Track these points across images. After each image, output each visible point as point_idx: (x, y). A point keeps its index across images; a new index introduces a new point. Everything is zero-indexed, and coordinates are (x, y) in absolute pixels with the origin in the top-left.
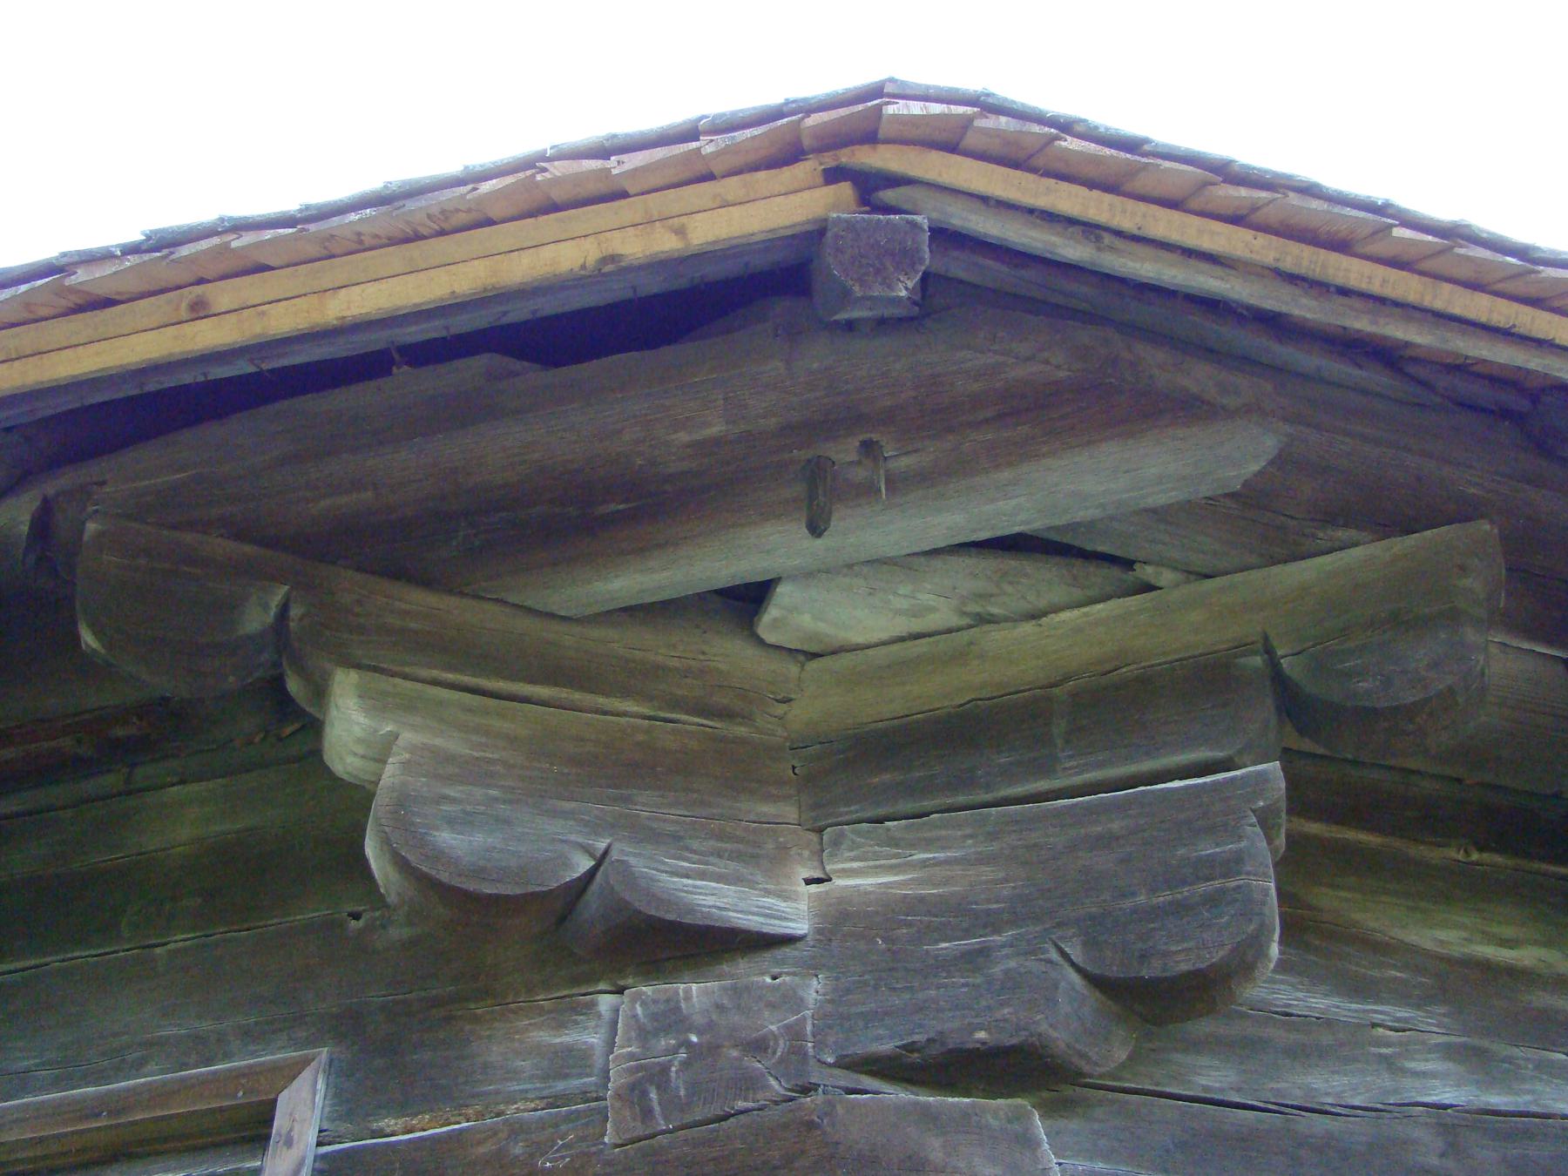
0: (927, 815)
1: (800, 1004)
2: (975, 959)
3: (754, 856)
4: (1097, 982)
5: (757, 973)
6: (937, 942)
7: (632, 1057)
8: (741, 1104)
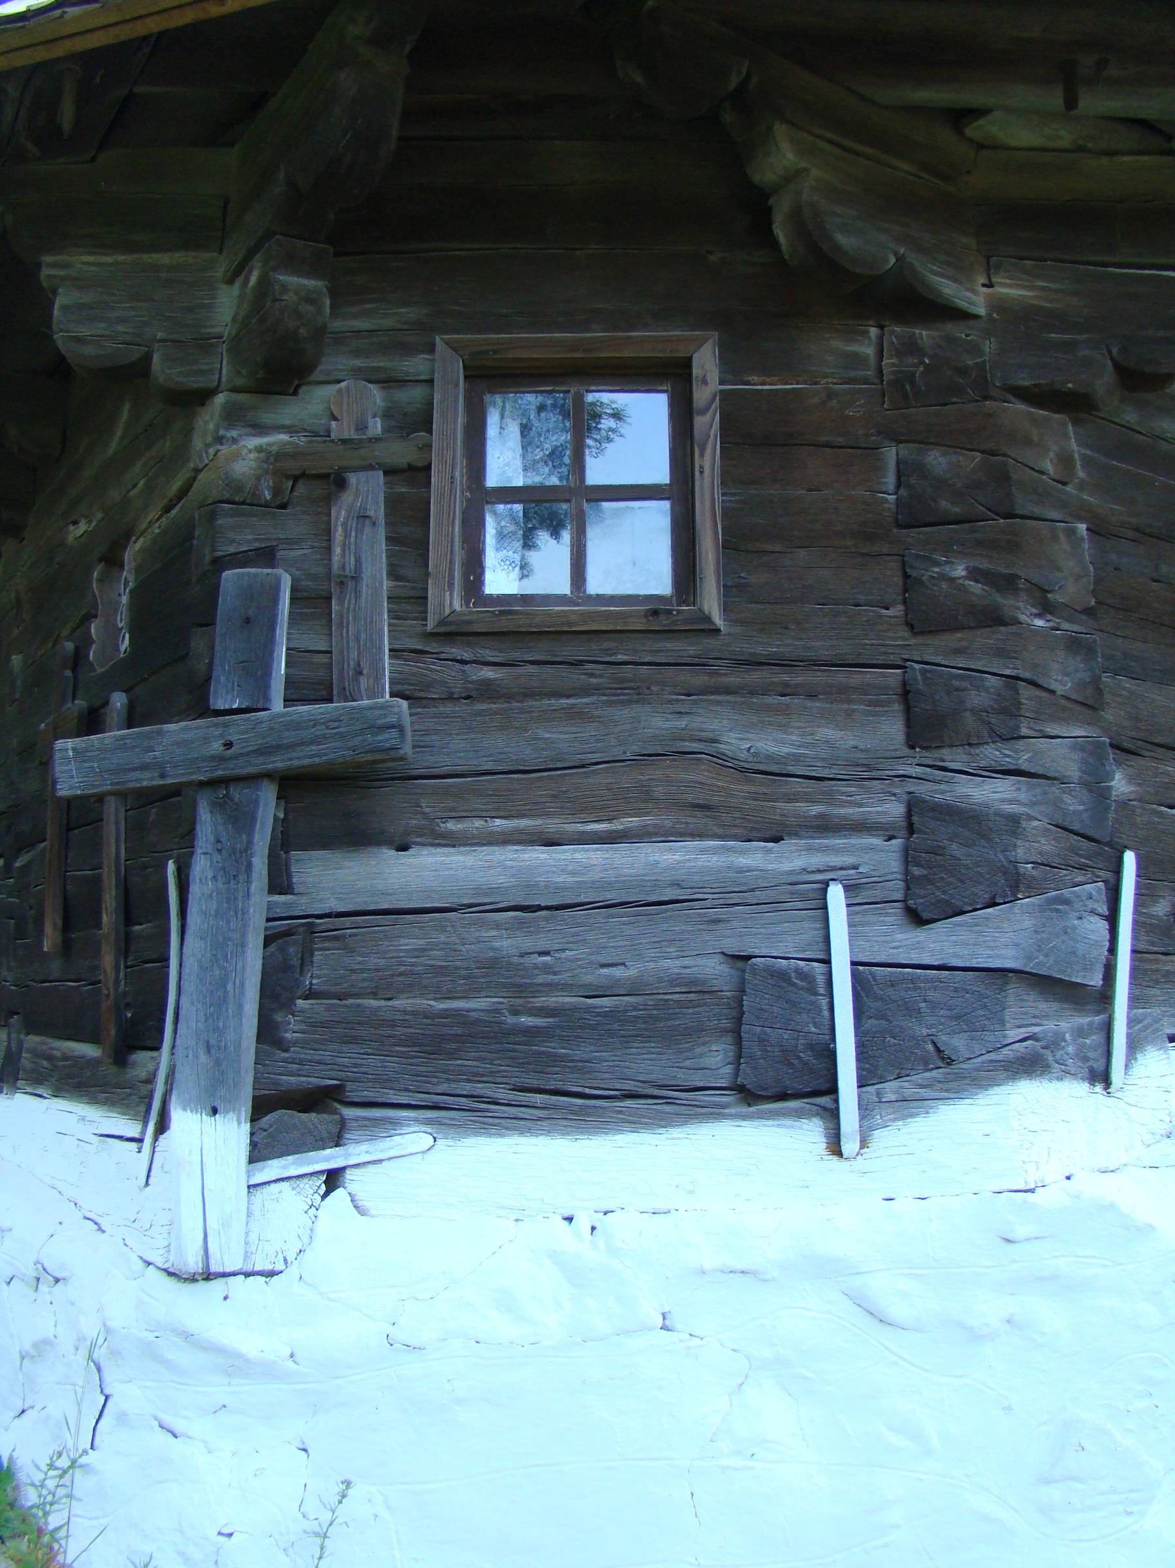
0: (1045, 260)
1: (980, 353)
2: (1070, 346)
3: (960, 269)
4: (1117, 366)
5: (959, 331)
6: (1050, 332)
7: (893, 365)
8: (955, 400)
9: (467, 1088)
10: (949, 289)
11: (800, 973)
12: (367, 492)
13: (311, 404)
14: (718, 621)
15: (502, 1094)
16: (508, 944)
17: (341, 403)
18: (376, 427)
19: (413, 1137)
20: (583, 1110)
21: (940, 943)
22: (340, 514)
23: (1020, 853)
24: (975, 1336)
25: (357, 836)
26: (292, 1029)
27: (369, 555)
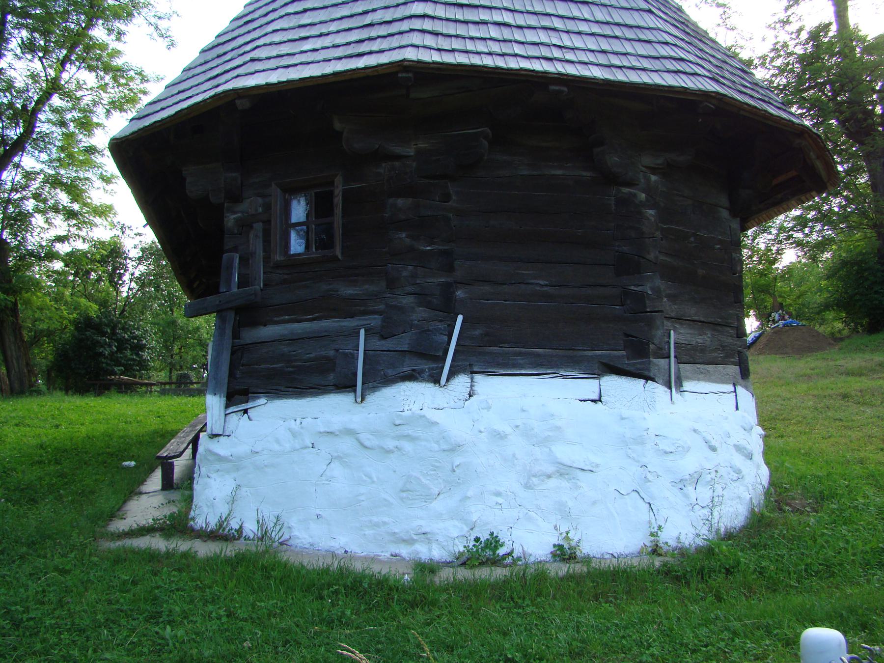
9: (275, 387)
10: (399, 150)
11: (351, 354)
12: (259, 226)
13: (244, 206)
14: (340, 257)
15: (283, 389)
16: (286, 349)
17: (251, 205)
18: (260, 210)
19: (263, 401)
20: (301, 392)
21: (388, 344)
22: (251, 236)
23: (414, 317)
24: (389, 452)
25: (256, 323)
26: (238, 374)
27: (257, 246)
